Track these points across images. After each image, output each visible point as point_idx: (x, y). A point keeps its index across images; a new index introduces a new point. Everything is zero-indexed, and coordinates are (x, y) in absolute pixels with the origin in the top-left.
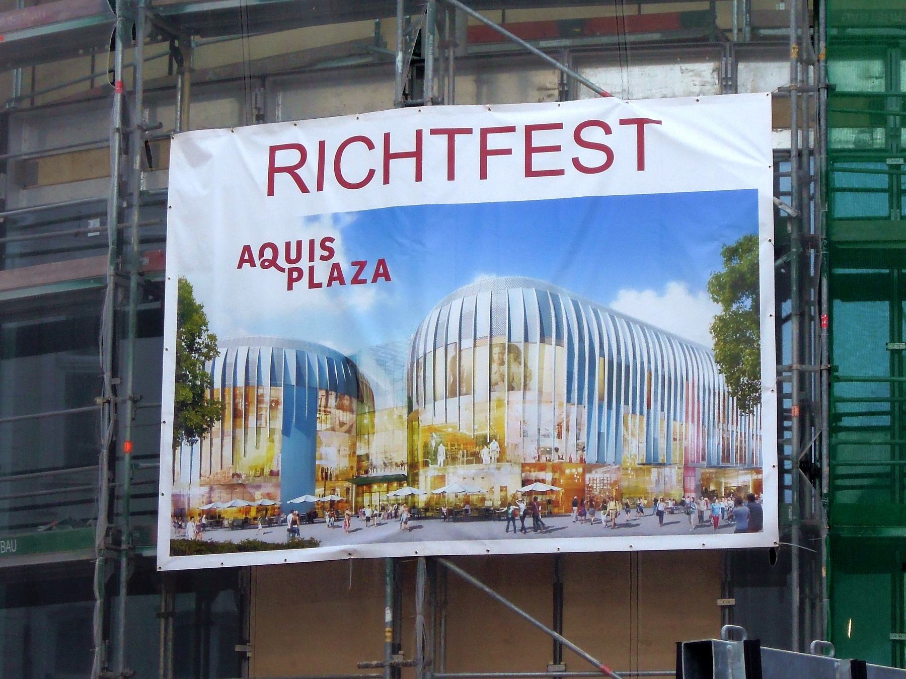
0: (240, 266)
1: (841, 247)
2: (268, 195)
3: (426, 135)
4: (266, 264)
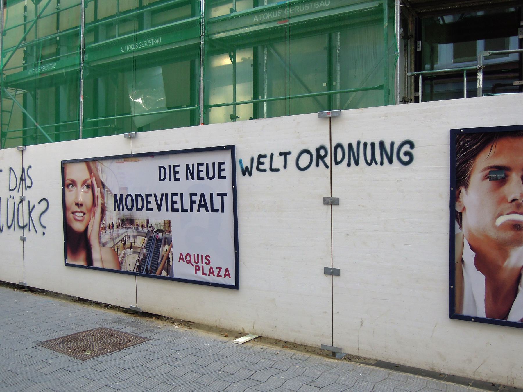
0: (179, 261)
2: (152, 211)
4: (188, 262)
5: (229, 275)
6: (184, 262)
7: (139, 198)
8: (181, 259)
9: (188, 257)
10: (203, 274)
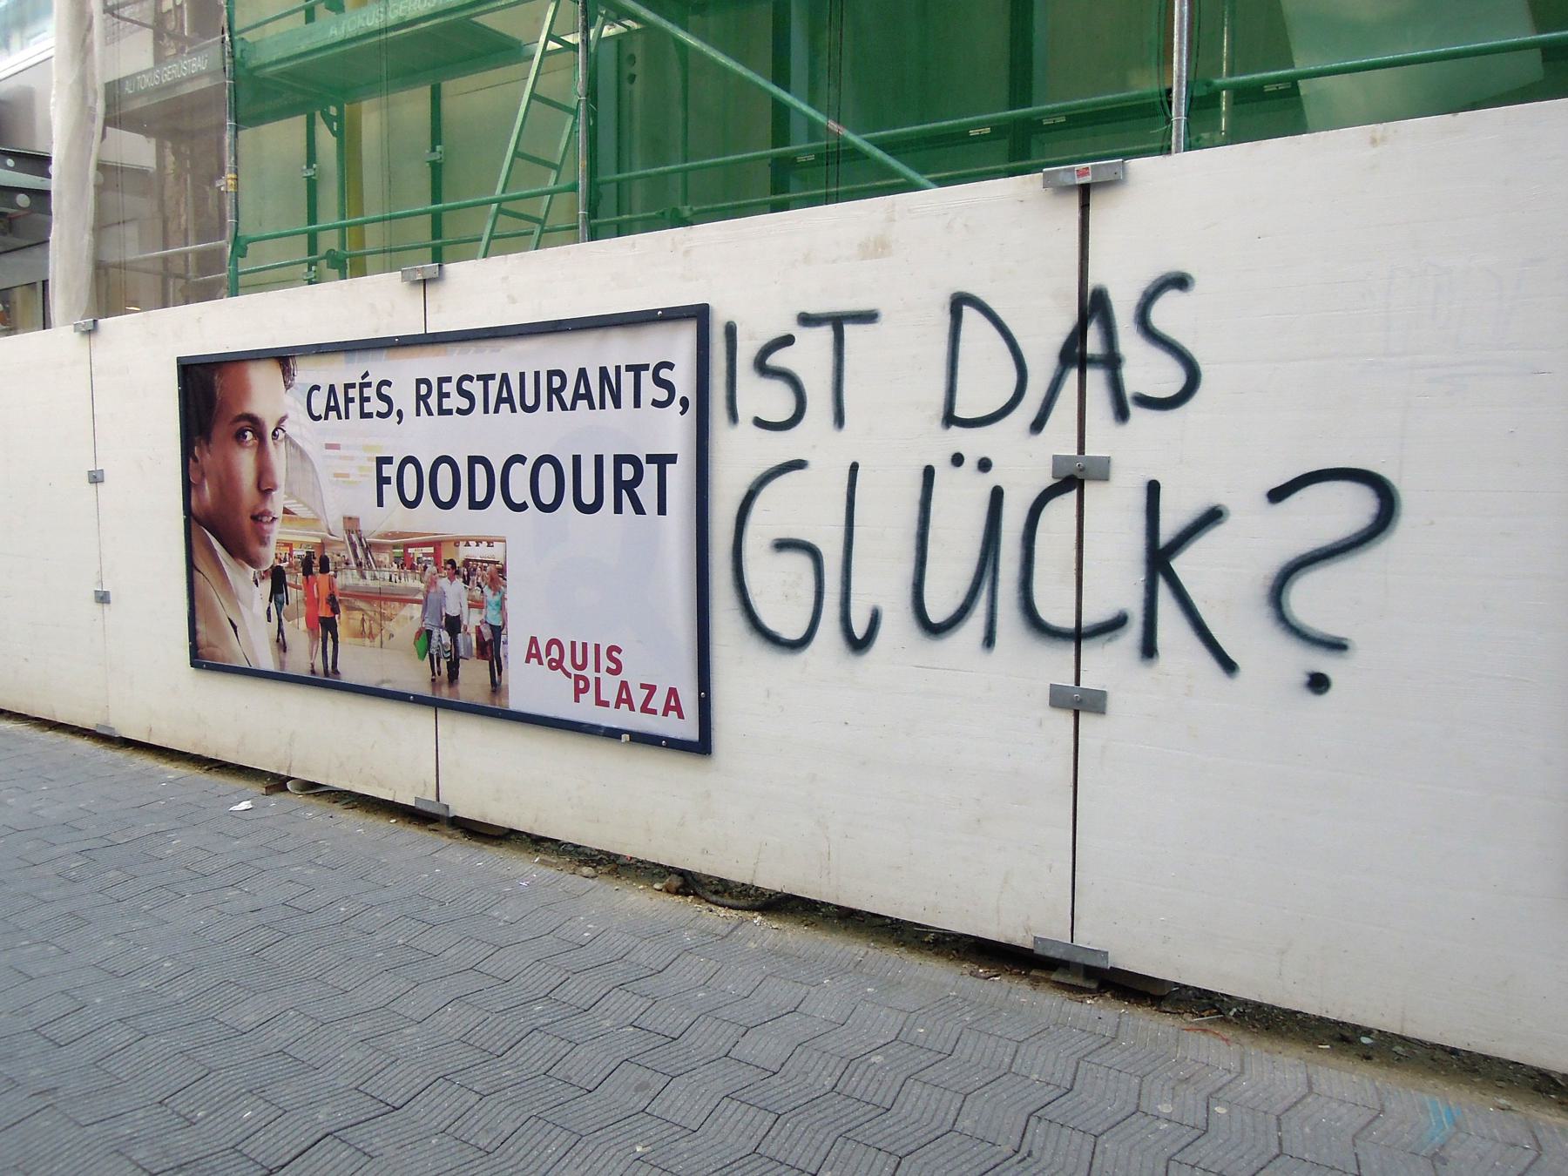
0: (528, 661)
1: (315, 586)
3: (623, 369)
4: (554, 664)
5: (678, 709)
6: (542, 664)
7: (480, 470)
8: (533, 654)
9: (555, 649)
10: (600, 702)
